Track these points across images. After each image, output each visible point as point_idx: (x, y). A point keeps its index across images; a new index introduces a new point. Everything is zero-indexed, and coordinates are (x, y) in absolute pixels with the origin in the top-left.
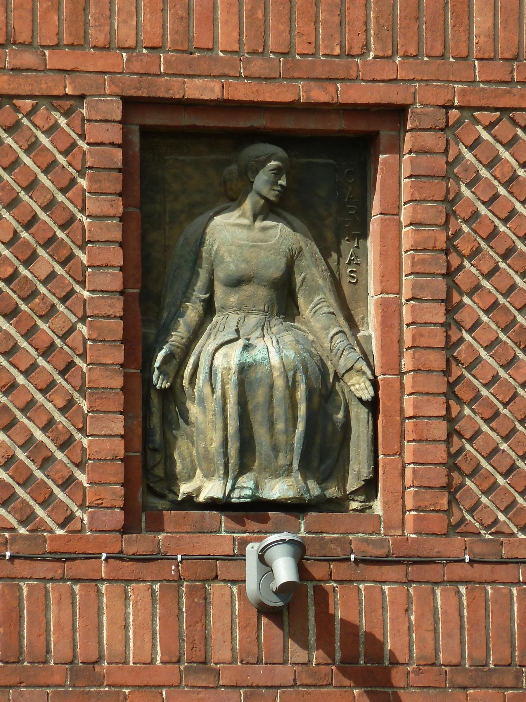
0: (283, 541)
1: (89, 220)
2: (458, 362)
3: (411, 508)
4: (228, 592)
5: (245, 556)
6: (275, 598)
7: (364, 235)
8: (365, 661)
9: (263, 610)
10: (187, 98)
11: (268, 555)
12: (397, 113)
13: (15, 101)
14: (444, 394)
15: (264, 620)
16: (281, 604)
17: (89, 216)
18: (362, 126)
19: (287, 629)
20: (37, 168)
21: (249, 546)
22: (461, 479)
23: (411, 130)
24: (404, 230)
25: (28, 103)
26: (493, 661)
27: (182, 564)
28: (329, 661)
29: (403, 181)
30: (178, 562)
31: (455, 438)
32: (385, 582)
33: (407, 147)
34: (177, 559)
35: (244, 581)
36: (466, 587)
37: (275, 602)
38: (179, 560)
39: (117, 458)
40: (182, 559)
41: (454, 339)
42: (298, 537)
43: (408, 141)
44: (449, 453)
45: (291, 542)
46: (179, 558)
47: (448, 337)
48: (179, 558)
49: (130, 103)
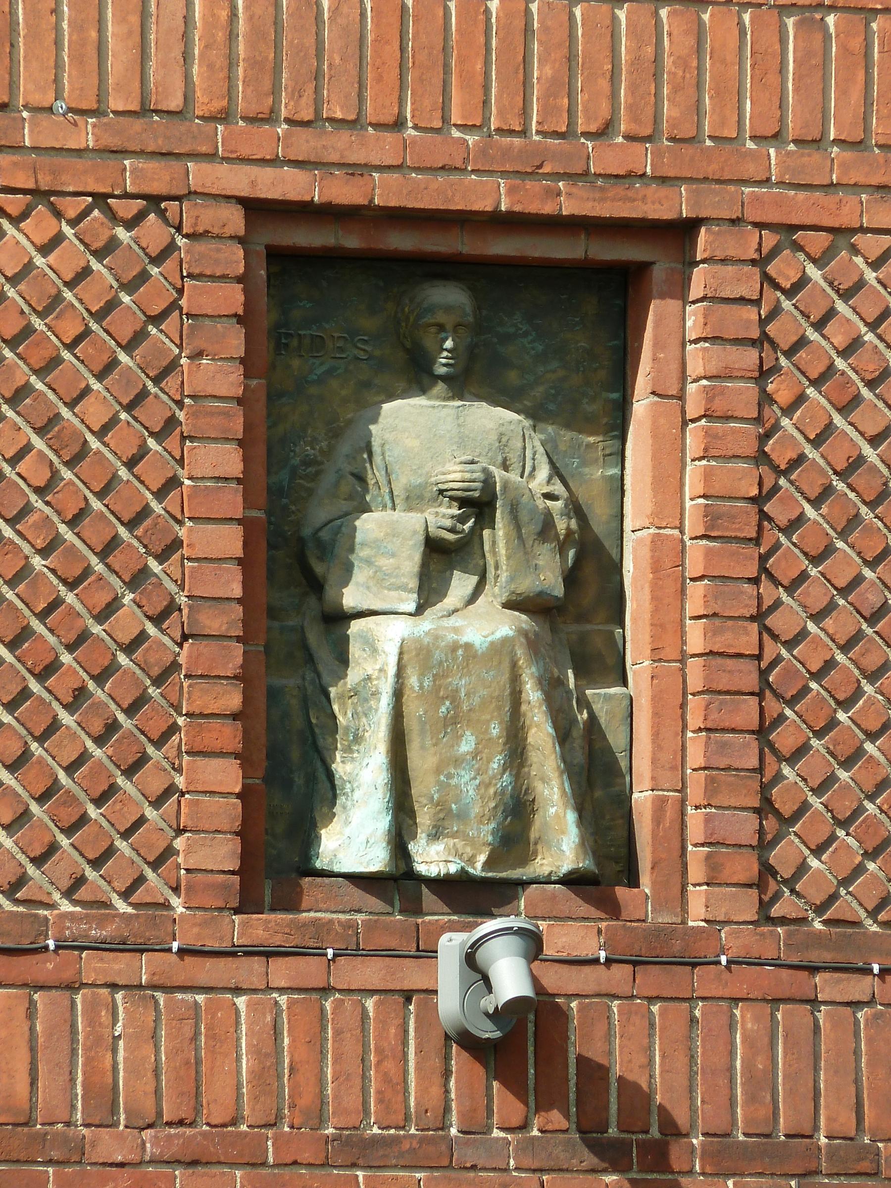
1: (184, 240)
2: (775, 637)
3: (700, 371)
6: (489, 1025)
8: (631, 1134)
9: (467, 1041)
11: (481, 955)
12: (684, 231)
14: (756, 811)
16: (498, 1034)
17: (187, 236)
20: (47, 631)
21: (444, 939)
22: (776, 767)
23: (704, 261)
24: (689, 347)
27: (334, 962)
29: (688, 504)
30: (329, 960)
31: (772, 882)
33: (696, 292)
34: (326, 955)
35: (435, 992)
37: (488, 1031)
38: (330, 957)
40: (335, 955)
41: (767, 602)
43: (700, 280)
44: (761, 900)
45: (521, 932)
46: (330, 952)
47: (761, 831)
48: (330, 952)
49: (256, 209)
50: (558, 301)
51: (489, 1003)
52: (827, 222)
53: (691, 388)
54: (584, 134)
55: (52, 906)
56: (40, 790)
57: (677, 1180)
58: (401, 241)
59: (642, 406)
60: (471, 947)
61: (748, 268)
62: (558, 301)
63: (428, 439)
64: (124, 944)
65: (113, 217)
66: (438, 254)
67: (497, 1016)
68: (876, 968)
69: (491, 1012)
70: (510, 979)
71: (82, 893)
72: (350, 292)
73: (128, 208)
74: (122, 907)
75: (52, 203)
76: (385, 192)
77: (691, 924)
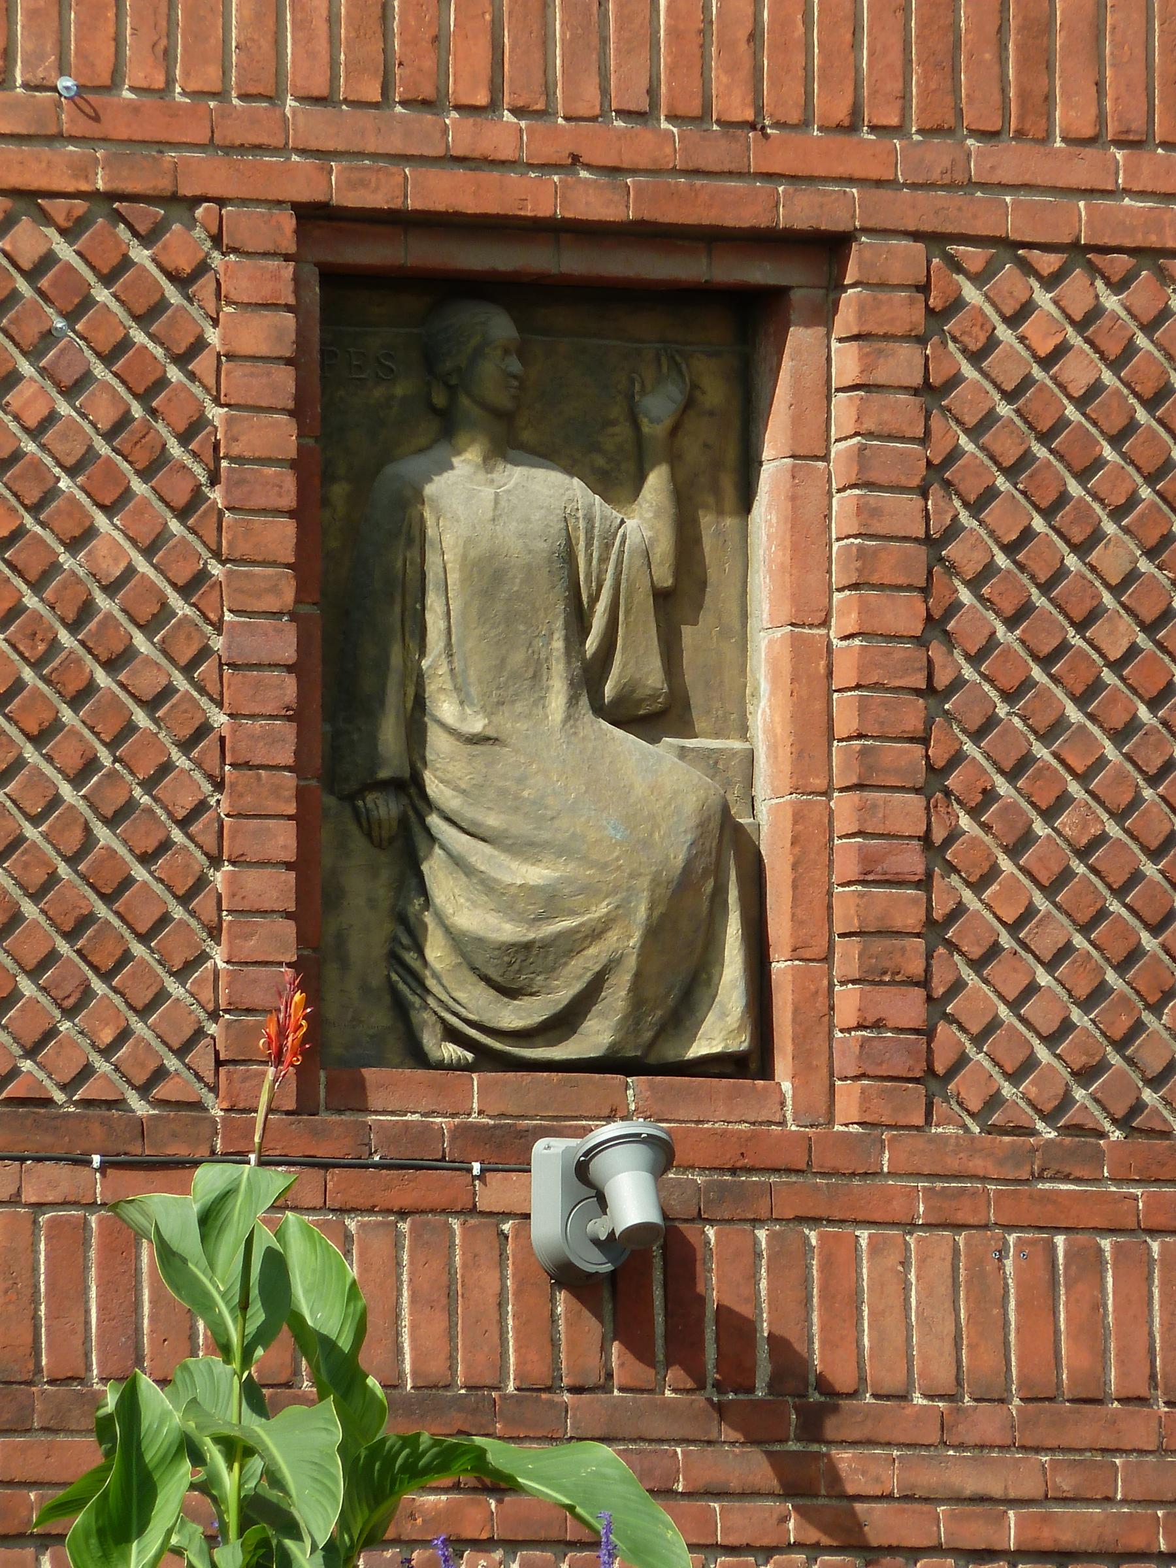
0: (634, 1138)
4: (945, 1251)
5: (529, 1164)
7: (745, 503)
9: (565, 1275)
10: (785, 229)
11: (599, 1165)
12: (829, 247)
13: (952, 249)
15: (562, 1296)
18: (759, 272)
19: (608, 1317)
21: (540, 1146)
23: (853, 285)
25: (1048, 262)
26: (1019, 1389)
28: (690, 1384)
32: (1058, 1230)
34: (470, 1170)
36: (462, 1220)
37: (596, 1263)
39: (898, 978)
42: (661, 1129)
45: (650, 1140)
46: (476, 1167)
49: (313, 216)
50: (651, 331)
51: (600, 1228)
52: (1128, 243)
53: (836, 449)
54: (345, 101)
55: (1103, 1135)
56: (1082, 992)
57: (827, 1455)
58: (574, 262)
59: (773, 470)
60: (585, 1154)
61: (273, 264)
62: (651, 331)
63: (484, 506)
64: (360, 1158)
65: (1027, 268)
66: (494, 273)
67: (608, 1244)
68: (96, 1159)
69: (603, 1238)
70: (632, 1201)
71: (161, 1091)
72: (427, 321)
73: (1048, 262)
74: (140, 1107)
75: (1159, 266)
76: (539, 197)
77: (837, 1128)
